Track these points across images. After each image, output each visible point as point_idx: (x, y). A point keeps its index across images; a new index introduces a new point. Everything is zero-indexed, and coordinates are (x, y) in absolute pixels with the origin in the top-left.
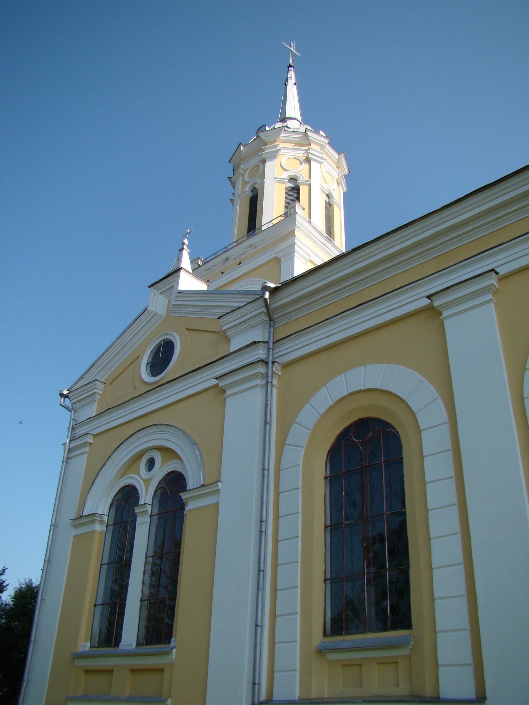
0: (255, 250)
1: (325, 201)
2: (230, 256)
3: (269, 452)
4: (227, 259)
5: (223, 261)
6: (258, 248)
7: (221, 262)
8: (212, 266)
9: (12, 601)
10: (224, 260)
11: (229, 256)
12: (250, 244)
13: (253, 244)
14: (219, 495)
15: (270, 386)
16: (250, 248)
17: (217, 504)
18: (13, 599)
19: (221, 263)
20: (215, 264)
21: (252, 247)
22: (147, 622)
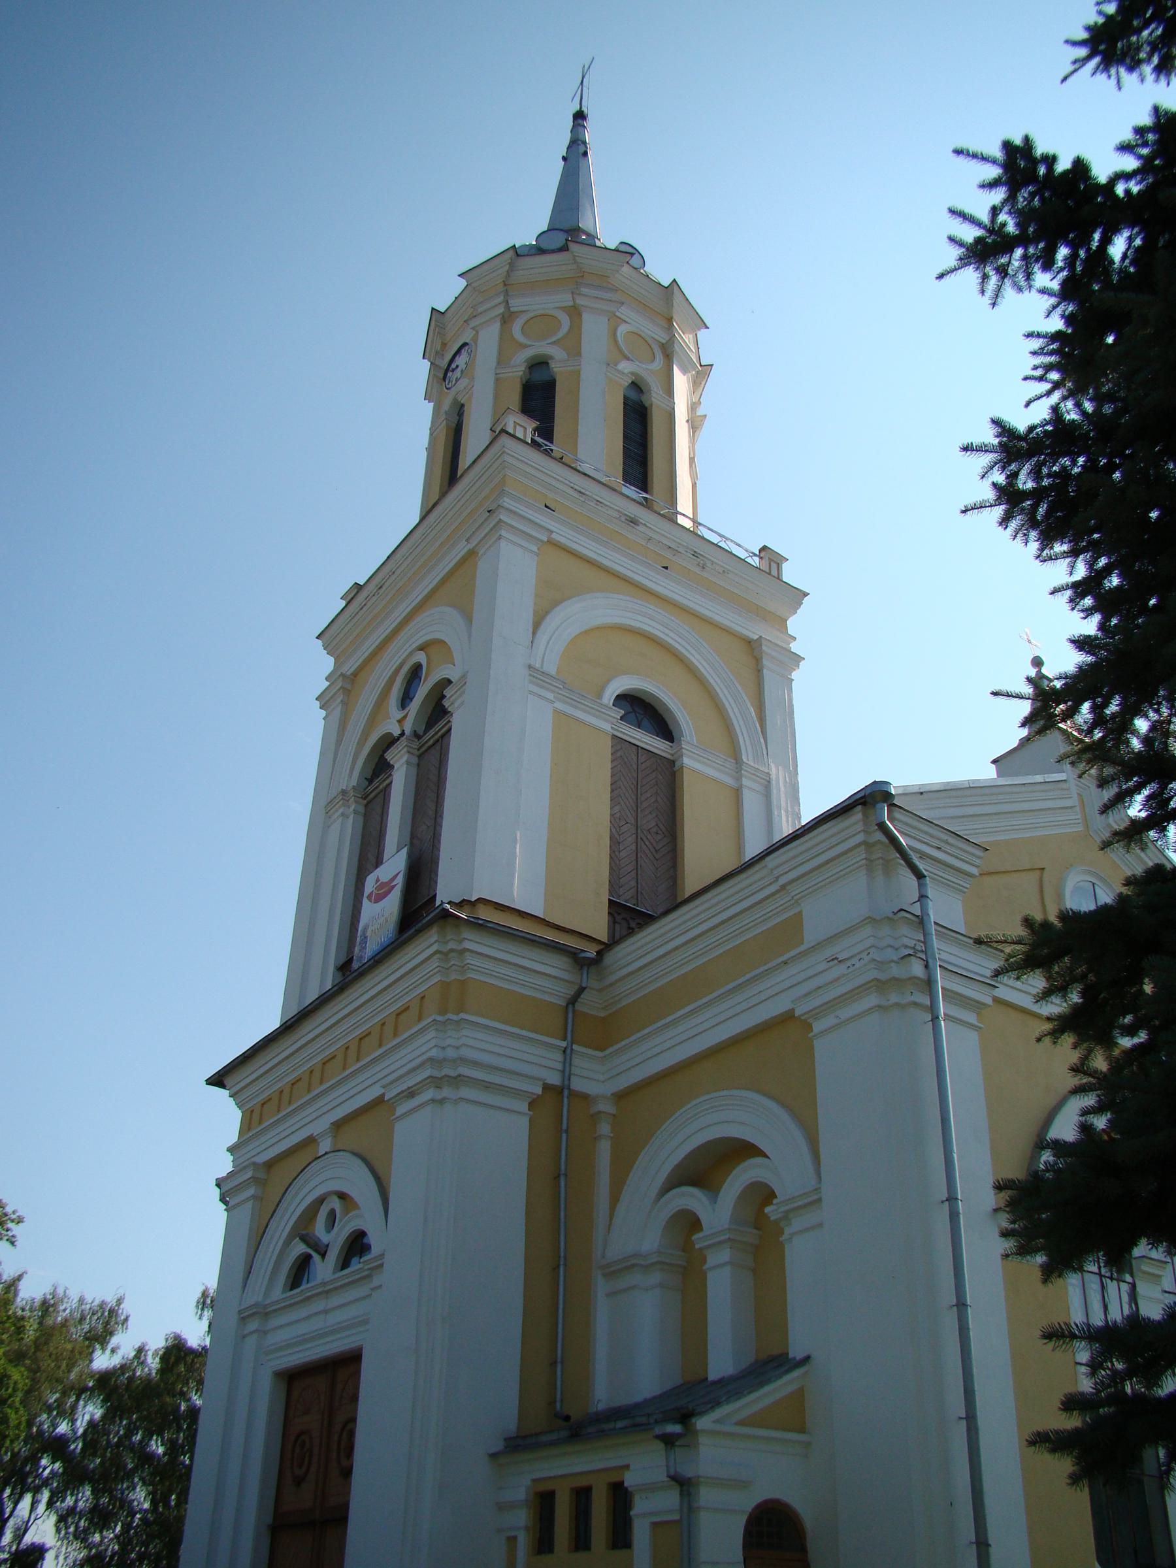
0: (697, 570)
1: (1024, 382)
2: (645, 525)
3: (633, 267)
4: (633, 522)
5: (626, 515)
6: (705, 574)
7: (619, 511)
8: (594, 496)
9: (1088, 612)
10: (627, 515)
11: (643, 522)
12: (699, 552)
13: (702, 555)
14: (876, 811)
15: (122, 1313)
16: (691, 556)
17: (800, 913)
18: (1088, 601)
19: (615, 514)
20: (603, 501)
21: (699, 560)
22: (674, 1117)
